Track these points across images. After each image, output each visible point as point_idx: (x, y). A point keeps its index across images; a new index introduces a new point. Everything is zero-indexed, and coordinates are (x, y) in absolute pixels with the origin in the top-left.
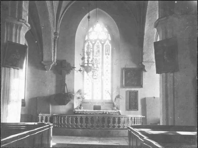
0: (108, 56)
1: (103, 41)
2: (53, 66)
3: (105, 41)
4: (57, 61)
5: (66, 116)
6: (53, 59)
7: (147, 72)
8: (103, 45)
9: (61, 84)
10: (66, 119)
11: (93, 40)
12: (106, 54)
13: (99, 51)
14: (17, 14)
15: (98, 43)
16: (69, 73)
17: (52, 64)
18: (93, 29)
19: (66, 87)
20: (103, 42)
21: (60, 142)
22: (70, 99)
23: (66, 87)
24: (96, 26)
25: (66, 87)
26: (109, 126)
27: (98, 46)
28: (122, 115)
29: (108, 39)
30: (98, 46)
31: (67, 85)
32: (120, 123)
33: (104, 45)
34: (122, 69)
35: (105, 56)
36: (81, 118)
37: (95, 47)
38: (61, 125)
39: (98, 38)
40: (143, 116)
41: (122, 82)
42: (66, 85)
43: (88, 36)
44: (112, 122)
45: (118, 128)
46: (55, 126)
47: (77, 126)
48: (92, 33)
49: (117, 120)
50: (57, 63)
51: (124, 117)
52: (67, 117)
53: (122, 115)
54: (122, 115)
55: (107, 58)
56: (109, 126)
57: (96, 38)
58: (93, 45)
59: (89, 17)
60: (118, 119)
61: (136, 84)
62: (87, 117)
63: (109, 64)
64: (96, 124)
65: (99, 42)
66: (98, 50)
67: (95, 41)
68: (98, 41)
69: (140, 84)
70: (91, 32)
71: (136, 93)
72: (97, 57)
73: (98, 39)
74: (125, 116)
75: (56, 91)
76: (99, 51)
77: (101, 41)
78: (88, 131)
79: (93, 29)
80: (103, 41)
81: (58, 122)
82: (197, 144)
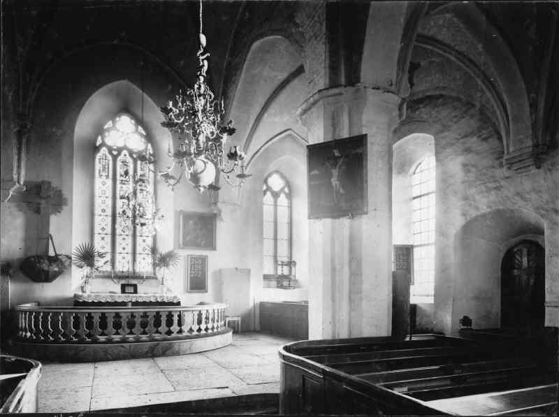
0: (107, 181)
1: (115, 150)
2: (18, 192)
4: (26, 183)
5: (60, 313)
6: (15, 177)
8: (115, 158)
9: (38, 233)
10: (41, 320)
11: (115, 148)
13: (126, 173)
15: (125, 155)
16: (59, 212)
17: (15, 187)
18: (114, 126)
19: (52, 241)
20: (115, 153)
22: (63, 269)
23: (50, 241)
24: (119, 120)
25: (52, 241)
26: (169, 333)
27: (125, 163)
28: (183, 307)
30: (125, 163)
31: (53, 238)
32: (172, 325)
36: (103, 317)
37: (119, 164)
38: (44, 335)
40: (463, 325)
42: (52, 239)
44: (176, 321)
45: (197, 333)
46: (26, 336)
47: (79, 336)
48: (113, 133)
49: (176, 319)
50: (27, 187)
51: (193, 311)
52: (42, 314)
53: (183, 307)
54: (184, 306)
55: (104, 184)
56: (169, 333)
57: (120, 144)
58: (115, 158)
60: (198, 315)
61: (203, 243)
62: (145, 315)
63: (107, 197)
64: (140, 328)
65: (128, 155)
66: (125, 169)
67: (120, 150)
68: (125, 152)
69: (211, 245)
70: (108, 130)
71: (204, 260)
72: (124, 184)
73: (125, 148)
74: (193, 309)
75: (27, 248)
76: (126, 173)
80: (115, 150)
81: (36, 325)
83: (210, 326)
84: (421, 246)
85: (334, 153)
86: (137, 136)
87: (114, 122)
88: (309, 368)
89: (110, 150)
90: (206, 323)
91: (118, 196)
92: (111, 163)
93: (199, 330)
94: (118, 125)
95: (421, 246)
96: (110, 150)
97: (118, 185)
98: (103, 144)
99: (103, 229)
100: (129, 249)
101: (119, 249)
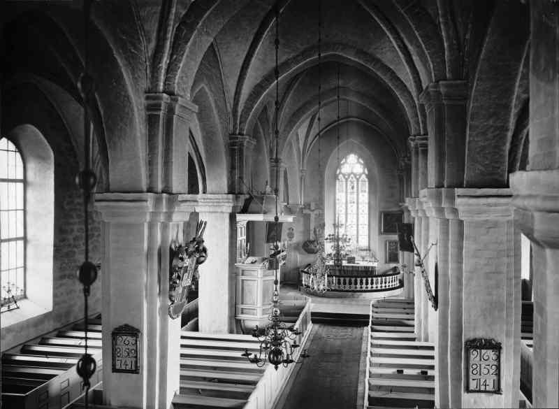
3: (360, 175)
7: (266, 371)
8: (358, 180)
12: (362, 191)
14: (161, 128)
20: (358, 177)
21: (201, 143)
27: (352, 182)
29: (364, 173)
30: (352, 182)
33: (360, 180)
34: (381, 213)
35: (360, 195)
39: (357, 163)
41: (380, 229)
43: (340, 169)
48: (346, 165)
57: (349, 171)
59: (339, 149)
67: (349, 175)
68: (352, 176)
70: (344, 163)
73: (352, 173)
77: (355, 175)
78: (470, 279)
79: (346, 161)
82: (416, 308)
83: (390, 284)
84: (9, 240)
85: (537, 119)
86: (359, 165)
87: (346, 158)
88: (420, 292)
89: (344, 175)
90: (385, 283)
91: (349, 202)
92: (344, 183)
93: (386, 286)
94: (348, 161)
95: (9, 240)
96: (344, 175)
97: (349, 196)
98: (340, 173)
99: (363, 227)
100: (355, 211)
101: (360, 211)
